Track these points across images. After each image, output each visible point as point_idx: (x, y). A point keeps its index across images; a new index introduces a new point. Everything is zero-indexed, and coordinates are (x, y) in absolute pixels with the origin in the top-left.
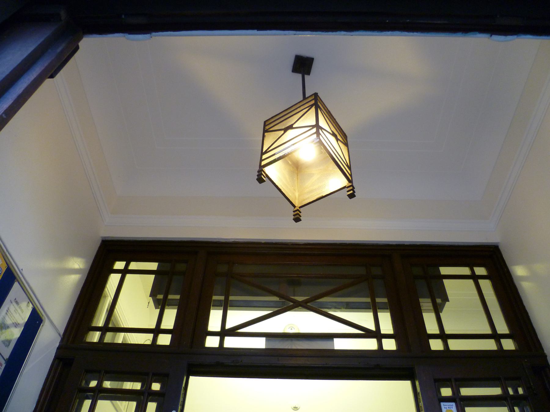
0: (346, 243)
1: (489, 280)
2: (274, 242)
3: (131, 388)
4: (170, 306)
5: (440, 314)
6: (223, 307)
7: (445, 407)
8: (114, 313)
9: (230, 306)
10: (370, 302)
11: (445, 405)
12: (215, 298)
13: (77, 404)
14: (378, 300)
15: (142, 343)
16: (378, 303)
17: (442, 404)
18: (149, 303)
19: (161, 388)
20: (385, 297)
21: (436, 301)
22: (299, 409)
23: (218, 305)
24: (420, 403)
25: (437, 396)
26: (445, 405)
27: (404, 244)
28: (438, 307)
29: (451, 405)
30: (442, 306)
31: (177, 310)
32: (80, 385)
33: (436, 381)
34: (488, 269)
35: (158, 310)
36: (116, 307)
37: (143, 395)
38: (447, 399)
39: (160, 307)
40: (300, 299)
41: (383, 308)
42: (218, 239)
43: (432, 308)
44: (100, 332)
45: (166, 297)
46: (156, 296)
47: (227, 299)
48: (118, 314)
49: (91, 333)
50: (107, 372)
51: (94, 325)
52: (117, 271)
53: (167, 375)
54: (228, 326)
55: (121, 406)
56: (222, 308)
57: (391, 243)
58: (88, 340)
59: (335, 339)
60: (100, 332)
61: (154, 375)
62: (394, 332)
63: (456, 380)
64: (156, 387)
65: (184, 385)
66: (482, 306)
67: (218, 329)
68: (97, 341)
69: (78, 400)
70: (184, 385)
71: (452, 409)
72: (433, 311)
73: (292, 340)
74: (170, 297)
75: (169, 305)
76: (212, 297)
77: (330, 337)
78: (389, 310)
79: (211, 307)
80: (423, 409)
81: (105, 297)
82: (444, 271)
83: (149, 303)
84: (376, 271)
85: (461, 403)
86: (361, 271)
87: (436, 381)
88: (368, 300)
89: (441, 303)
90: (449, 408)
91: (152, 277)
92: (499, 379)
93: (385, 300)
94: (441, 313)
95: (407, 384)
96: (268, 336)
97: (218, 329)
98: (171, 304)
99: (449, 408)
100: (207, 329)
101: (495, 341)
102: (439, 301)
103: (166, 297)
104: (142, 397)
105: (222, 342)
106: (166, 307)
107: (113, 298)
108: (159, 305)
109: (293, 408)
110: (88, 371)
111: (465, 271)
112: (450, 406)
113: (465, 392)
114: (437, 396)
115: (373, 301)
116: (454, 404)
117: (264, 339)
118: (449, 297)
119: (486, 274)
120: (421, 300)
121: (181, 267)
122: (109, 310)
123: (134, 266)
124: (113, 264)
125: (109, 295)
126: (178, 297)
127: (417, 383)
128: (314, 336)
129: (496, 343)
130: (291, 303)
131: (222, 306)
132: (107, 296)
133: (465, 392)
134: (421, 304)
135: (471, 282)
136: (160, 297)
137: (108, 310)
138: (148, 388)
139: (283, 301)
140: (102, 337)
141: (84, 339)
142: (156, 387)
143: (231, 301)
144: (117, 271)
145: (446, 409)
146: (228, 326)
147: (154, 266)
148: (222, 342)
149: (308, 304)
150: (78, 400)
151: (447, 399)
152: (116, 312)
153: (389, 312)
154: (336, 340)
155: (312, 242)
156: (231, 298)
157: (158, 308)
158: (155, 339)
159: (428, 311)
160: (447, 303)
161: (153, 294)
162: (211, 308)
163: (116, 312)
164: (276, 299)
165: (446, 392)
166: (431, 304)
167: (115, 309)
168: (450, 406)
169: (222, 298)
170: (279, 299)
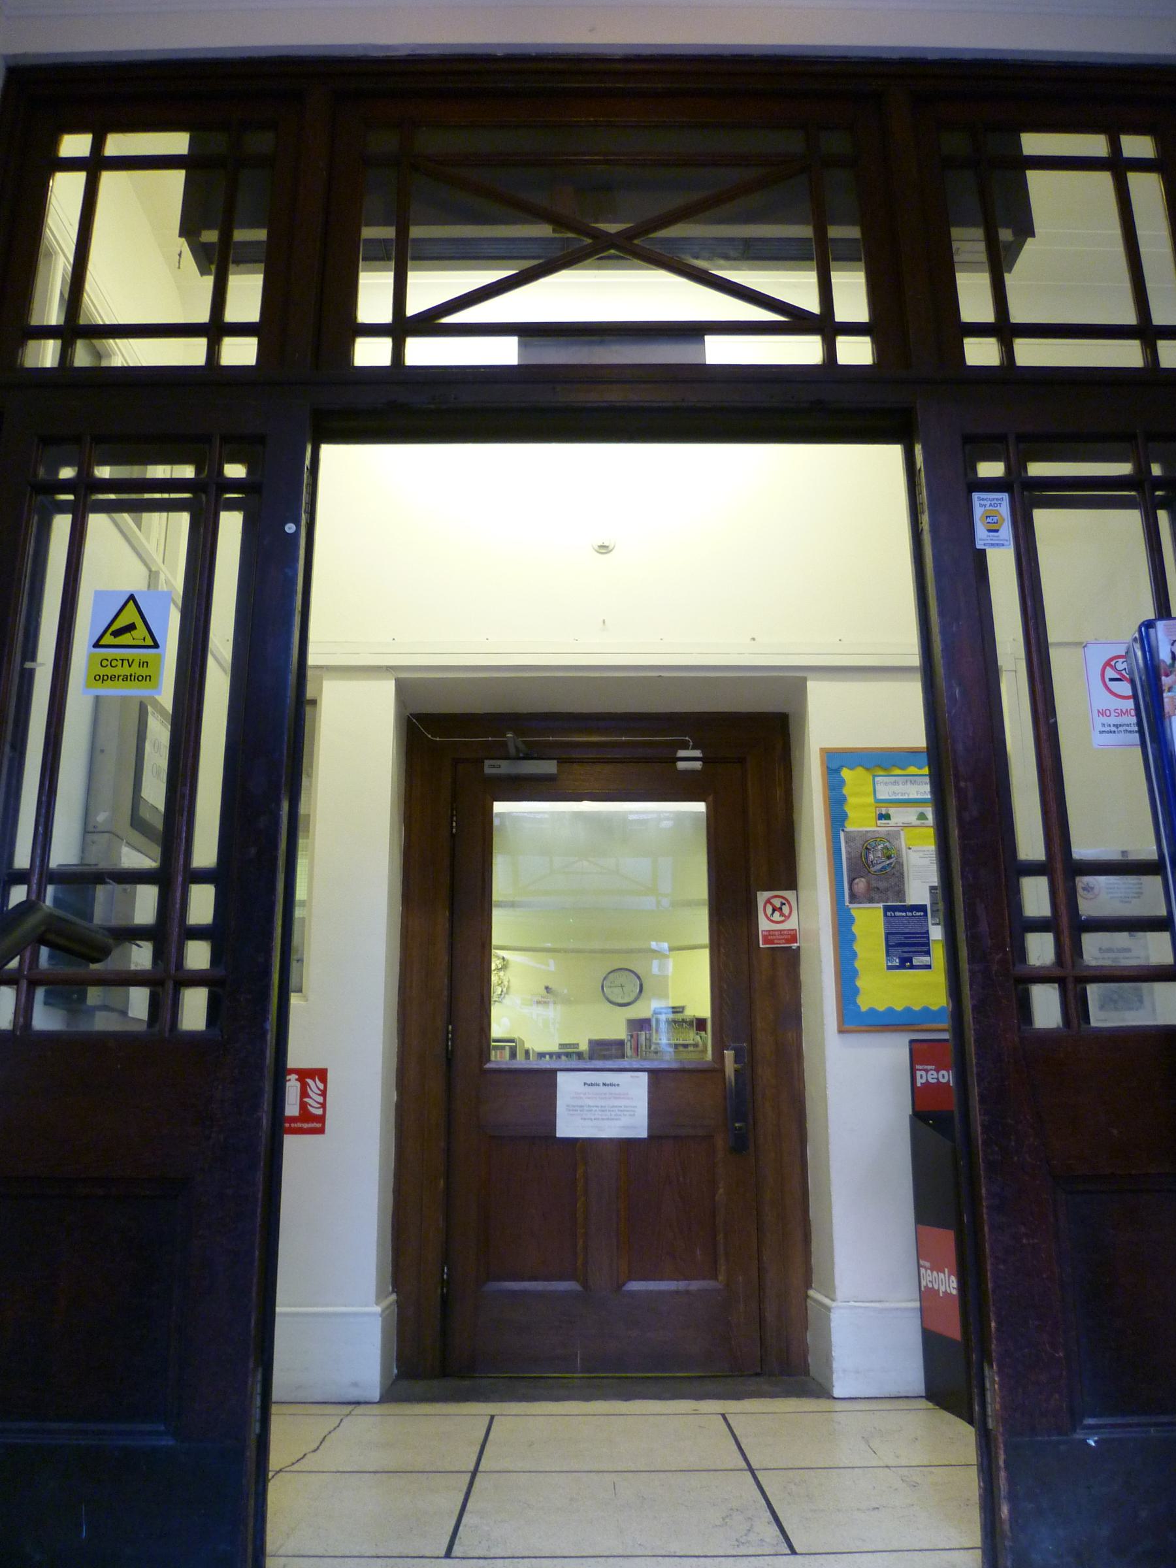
0: (752, 56)
1: (1152, 136)
2: (533, 52)
3: (168, 477)
4: (241, 265)
5: (1006, 275)
6: (393, 263)
7: (982, 502)
8: (83, 306)
9: (414, 258)
10: (810, 239)
11: (983, 499)
12: (369, 232)
13: (34, 529)
14: (834, 232)
15: (169, 733)
16: (834, 240)
17: (975, 496)
18: (180, 255)
19: (249, 473)
20: (853, 224)
21: (997, 233)
22: (611, 551)
23: (378, 254)
24: (919, 494)
25: (966, 475)
26: (983, 499)
27: (922, 56)
28: (1003, 253)
29: (997, 499)
30: (1015, 250)
31: (261, 276)
32: (35, 475)
33: (968, 439)
34: (1160, 145)
35: (209, 281)
36: (87, 287)
37: (205, 492)
38: (991, 485)
39: (213, 268)
40: (612, 228)
41: (847, 256)
42: (364, 46)
43: (983, 257)
44: (59, 342)
45: (226, 236)
46: (199, 235)
47: (402, 233)
48: (94, 306)
49: (32, 344)
50: (99, 440)
51: (35, 321)
52: (72, 164)
53: (261, 440)
54: (412, 309)
55: (149, 543)
56: (392, 264)
57: (885, 55)
58: (30, 362)
59: (708, 338)
60: (59, 342)
61: (225, 439)
62: (870, 319)
63: (1020, 438)
64: (235, 471)
65: (307, 462)
66: (1126, 255)
67: (385, 316)
68: (56, 365)
69: (36, 518)
70: (307, 462)
71: (998, 508)
72: (986, 266)
73: (591, 343)
74: (241, 235)
75: (237, 262)
76: (359, 232)
77: (696, 331)
78: (862, 264)
79: (361, 263)
80: (926, 507)
81: (49, 255)
82: (1034, 143)
83: (180, 255)
84: (836, 143)
85: (1025, 493)
86: (790, 142)
87: (968, 439)
88: (805, 231)
89: (1012, 242)
90: (991, 505)
91: (176, 179)
92: (1130, 438)
93: (854, 232)
94: (1010, 271)
95: (893, 453)
96: (525, 331)
97: (385, 316)
98: (245, 257)
99: (991, 505)
100: (356, 318)
101: (1142, 345)
102: (1005, 235)
103: (226, 236)
104: (204, 497)
105: (398, 352)
106: (232, 267)
107: (71, 260)
108: (211, 263)
109: (597, 548)
110: (48, 441)
111: (1095, 145)
112: (995, 502)
113: (1037, 469)
114: (966, 475)
115: (820, 232)
116: (1005, 496)
117: (512, 342)
118: (1036, 230)
119: (1153, 157)
120: (956, 232)
121: (260, 142)
122: (66, 296)
123: (117, 144)
124: (55, 144)
125: (60, 251)
126: (261, 235)
127: (918, 449)
128: (651, 330)
129: (1142, 349)
130: (585, 239)
131: (389, 259)
132: (55, 252)
133: (1037, 469)
134: (955, 245)
135: (1103, 180)
136: (211, 236)
137: (67, 273)
138: (216, 473)
139: (563, 239)
140: (65, 354)
141: (19, 360)
142: (235, 471)
143: (414, 240)
144: (72, 164)
145: (983, 509)
146: (412, 309)
147: (177, 143)
148: (398, 352)
149: (636, 242)
150: (36, 518)
151: (991, 485)
152: (89, 302)
153: (864, 270)
154: (710, 340)
155: (648, 52)
156: (416, 232)
157: (209, 273)
158: (213, 352)
159: (972, 267)
160: (1029, 240)
161: (188, 229)
162: (360, 265)
163: (89, 302)
164: (544, 230)
165: (990, 469)
166: (982, 246)
167: (85, 295)
168: (995, 502)
169: (389, 232)
170: (554, 231)
